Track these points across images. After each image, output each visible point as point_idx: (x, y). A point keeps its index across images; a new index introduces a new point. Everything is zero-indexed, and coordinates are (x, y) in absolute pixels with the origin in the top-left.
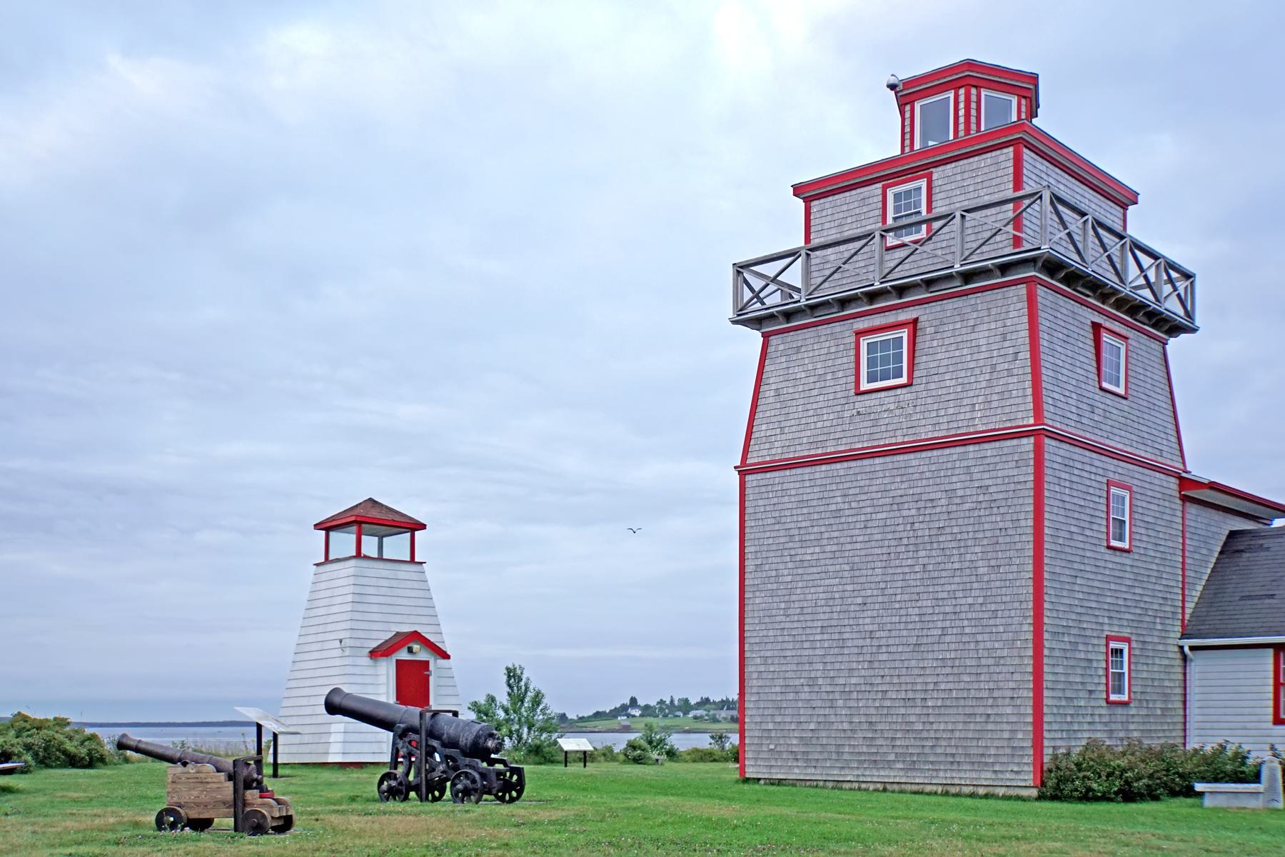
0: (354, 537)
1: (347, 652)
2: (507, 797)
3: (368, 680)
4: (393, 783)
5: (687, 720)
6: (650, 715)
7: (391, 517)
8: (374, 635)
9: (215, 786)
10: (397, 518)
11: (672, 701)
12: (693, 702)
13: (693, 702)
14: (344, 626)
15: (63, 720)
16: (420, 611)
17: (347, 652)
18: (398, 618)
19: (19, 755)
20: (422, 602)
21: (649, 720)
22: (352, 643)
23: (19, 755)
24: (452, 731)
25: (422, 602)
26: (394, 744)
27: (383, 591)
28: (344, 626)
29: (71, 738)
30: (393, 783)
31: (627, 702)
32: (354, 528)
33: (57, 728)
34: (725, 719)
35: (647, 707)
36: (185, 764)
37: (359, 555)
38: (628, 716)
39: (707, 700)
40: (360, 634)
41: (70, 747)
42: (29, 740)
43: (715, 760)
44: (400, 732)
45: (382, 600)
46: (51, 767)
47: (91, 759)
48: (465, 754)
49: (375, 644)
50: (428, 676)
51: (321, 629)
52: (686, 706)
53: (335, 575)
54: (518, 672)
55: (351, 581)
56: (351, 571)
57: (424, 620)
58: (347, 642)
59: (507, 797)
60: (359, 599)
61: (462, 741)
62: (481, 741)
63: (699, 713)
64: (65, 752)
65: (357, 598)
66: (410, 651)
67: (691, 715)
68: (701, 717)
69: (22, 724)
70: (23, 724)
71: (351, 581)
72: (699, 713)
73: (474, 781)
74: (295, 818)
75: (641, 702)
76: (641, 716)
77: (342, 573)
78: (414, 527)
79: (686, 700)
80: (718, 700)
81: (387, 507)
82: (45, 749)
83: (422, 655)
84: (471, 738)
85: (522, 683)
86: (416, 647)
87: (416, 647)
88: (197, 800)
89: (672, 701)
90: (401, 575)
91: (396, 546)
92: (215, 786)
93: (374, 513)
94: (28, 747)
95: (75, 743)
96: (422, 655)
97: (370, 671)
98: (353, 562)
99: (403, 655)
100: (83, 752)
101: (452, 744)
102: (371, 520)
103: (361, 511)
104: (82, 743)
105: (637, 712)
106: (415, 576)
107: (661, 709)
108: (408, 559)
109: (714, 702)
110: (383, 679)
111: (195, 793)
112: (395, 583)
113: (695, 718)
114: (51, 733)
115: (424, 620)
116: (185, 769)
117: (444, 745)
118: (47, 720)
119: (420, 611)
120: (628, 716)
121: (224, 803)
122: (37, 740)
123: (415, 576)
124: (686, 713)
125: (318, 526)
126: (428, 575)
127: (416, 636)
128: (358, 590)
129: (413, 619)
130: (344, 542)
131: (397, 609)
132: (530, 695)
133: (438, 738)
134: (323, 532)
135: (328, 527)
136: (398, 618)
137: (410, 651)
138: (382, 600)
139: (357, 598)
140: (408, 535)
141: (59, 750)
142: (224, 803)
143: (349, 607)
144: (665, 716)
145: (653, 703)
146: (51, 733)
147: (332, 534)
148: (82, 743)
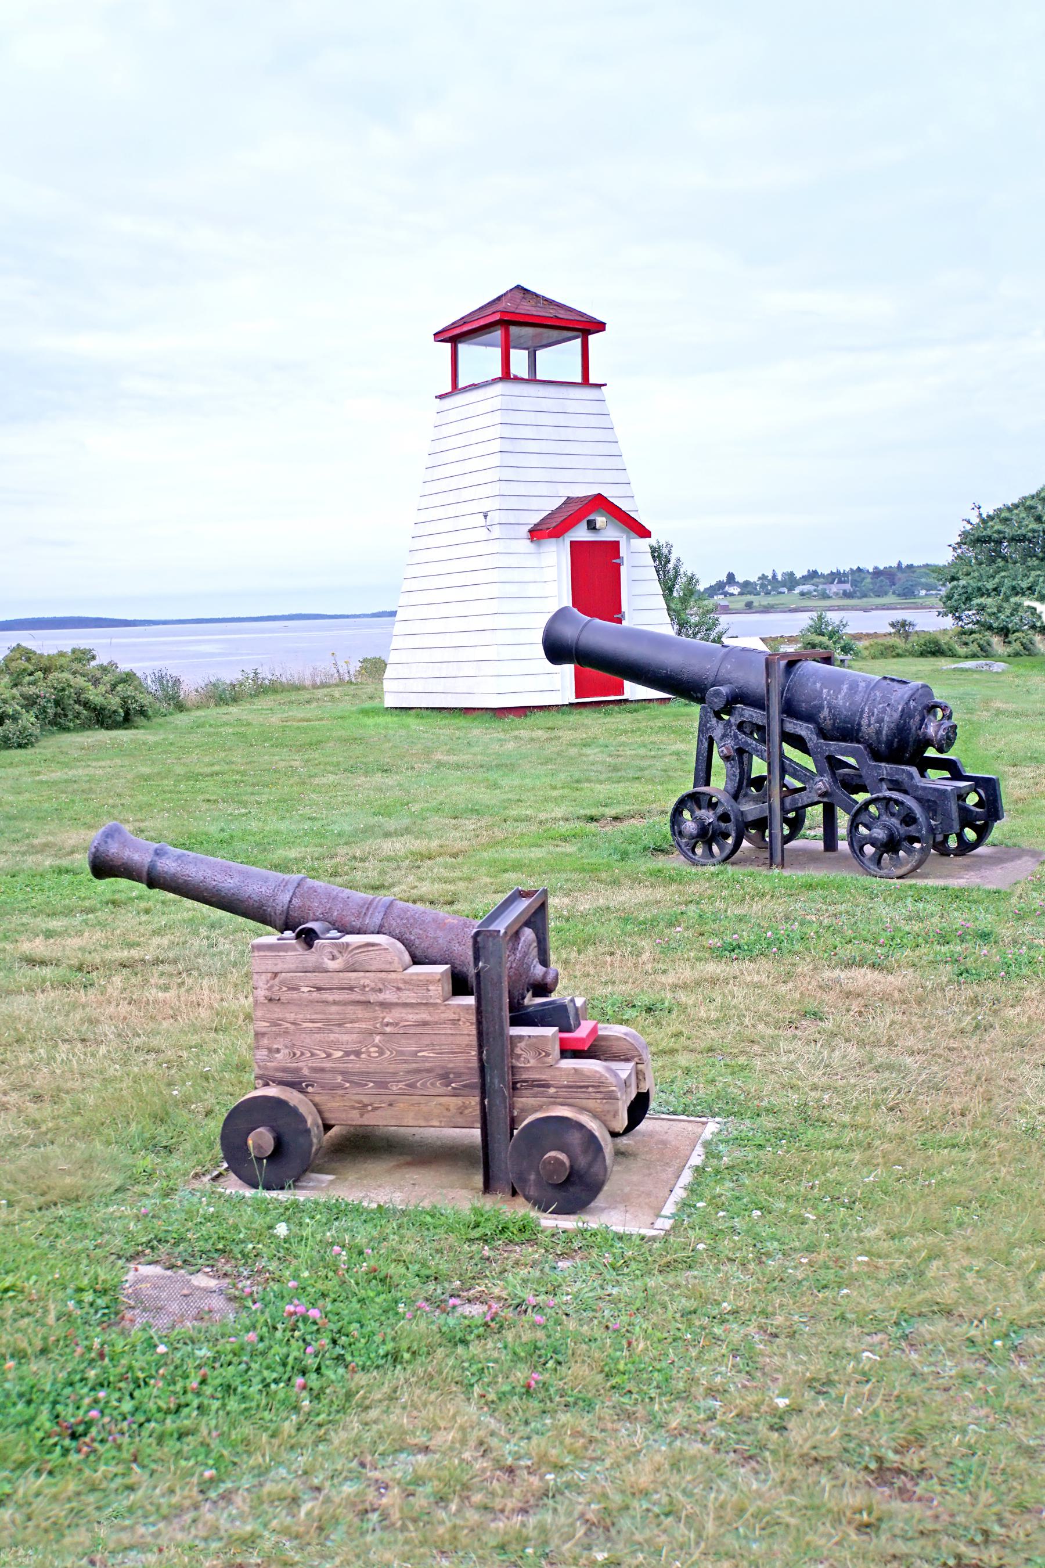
0: (497, 352)
1: (497, 531)
2: (953, 843)
3: (528, 575)
4: (709, 816)
5: (791, 598)
6: (750, 593)
7: (551, 312)
8: (535, 504)
9: (412, 1016)
10: (562, 314)
11: (774, 576)
12: (798, 575)
13: (798, 575)
14: (488, 490)
15: (84, 652)
16: (599, 462)
17: (497, 531)
18: (568, 476)
19: (15, 718)
20: (602, 449)
21: (749, 598)
22: (504, 517)
23: (15, 718)
24: (840, 700)
25: (602, 449)
26: (703, 728)
27: (545, 433)
28: (488, 490)
29: (96, 682)
30: (709, 816)
31: (724, 578)
32: (497, 334)
33: (76, 666)
34: (836, 594)
35: (747, 584)
36: (308, 937)
37: (506, 375)
38: (726, 594)
39: (815, 572)
40: (513, 503)
41: (95, 695)
42: (32, 690)
43: (898, 655)
44: (719, 703)
45: (545, 447)
46: (67, 729)
47: (127, 713)
48: (877, 756)
49: (536, 518)
50: (618, 566)
51: (452, 497)
52: (791, 581)
53: (471, 410)
54: (665, 551)
55: (497, 418)
56: (497, 403)
57: (608, 477)
58: (494, 517)
59: (953, 843)
60: (511, 446)
61: (868, 727)
62: (914, 723)
63: (805, 588)
64: (86, 704)
65: (508, 446)
66: (592, 526)
67: (797, 591)
68: (809, 593)
69: (25, 667)
70: (23, 664)
71: (497, 418)
72: (805, 588)
73: (909, 819)
74: (653, 1096)
75: (740, 579)
76: (740, 594)
77: (488, 406)
78: (587, 327)
79: (792, 574)
80: (826, 572)
81: (546, 300)
82: (57, 703)
83: (609, 531)
84: (891, 719)
85: (671, 565)
86: (600, 520)
87: (600, 520)
88: (354, 1064)
89: (774, 576)
90: (572, 406)
91: (560, 359)
92: (412, 1016)
93: (527, 308)
94: (30, 702)
95: (102, 689)
96: (609, 531)
97: (531, 561)
98: (500, 388)
99: (581, 533)
100: (114, 702)
101: (846, 731)
102: (522, 322)
103: (507, 305)
104: (114, 686)
105: (735, 590)
106: (594, 407)
107: (763, 586)
108: (580, 380)
109: (823, 575)
110: (551, 574)
111: (348, 1039)
112: (561, 419)
113: (802, 594)
114: (66, 675)
115: (608, 477)
116: (311, 957)
117: (822, 733)
118: (61, 654)
119: (599, 462)
120: (726, 594)
121: (446, 1077)
122: (42, 689)
123: (594, 407)
124: (790, 590)
125: (440, 336)
126: (611, 406)
127: (599, 502)
128: (508, 431)
129: (590, 476)
130: (481, 359)
131: (565, 461)
132: (681, 581)
133: (809, 717)
134: (448, 345)
135: (455, 336)
136: (568, 476)
137: (592, 526)
138: (545, 447)
139: (508, 446)
140: (578, 342)
141: (78, 702)
142: (446, 1077)
143: (496, 460)
144: (768, 593)
145: (753, 579)
146: (66, 675)
147: (462, 347)
148: (114, 686)
